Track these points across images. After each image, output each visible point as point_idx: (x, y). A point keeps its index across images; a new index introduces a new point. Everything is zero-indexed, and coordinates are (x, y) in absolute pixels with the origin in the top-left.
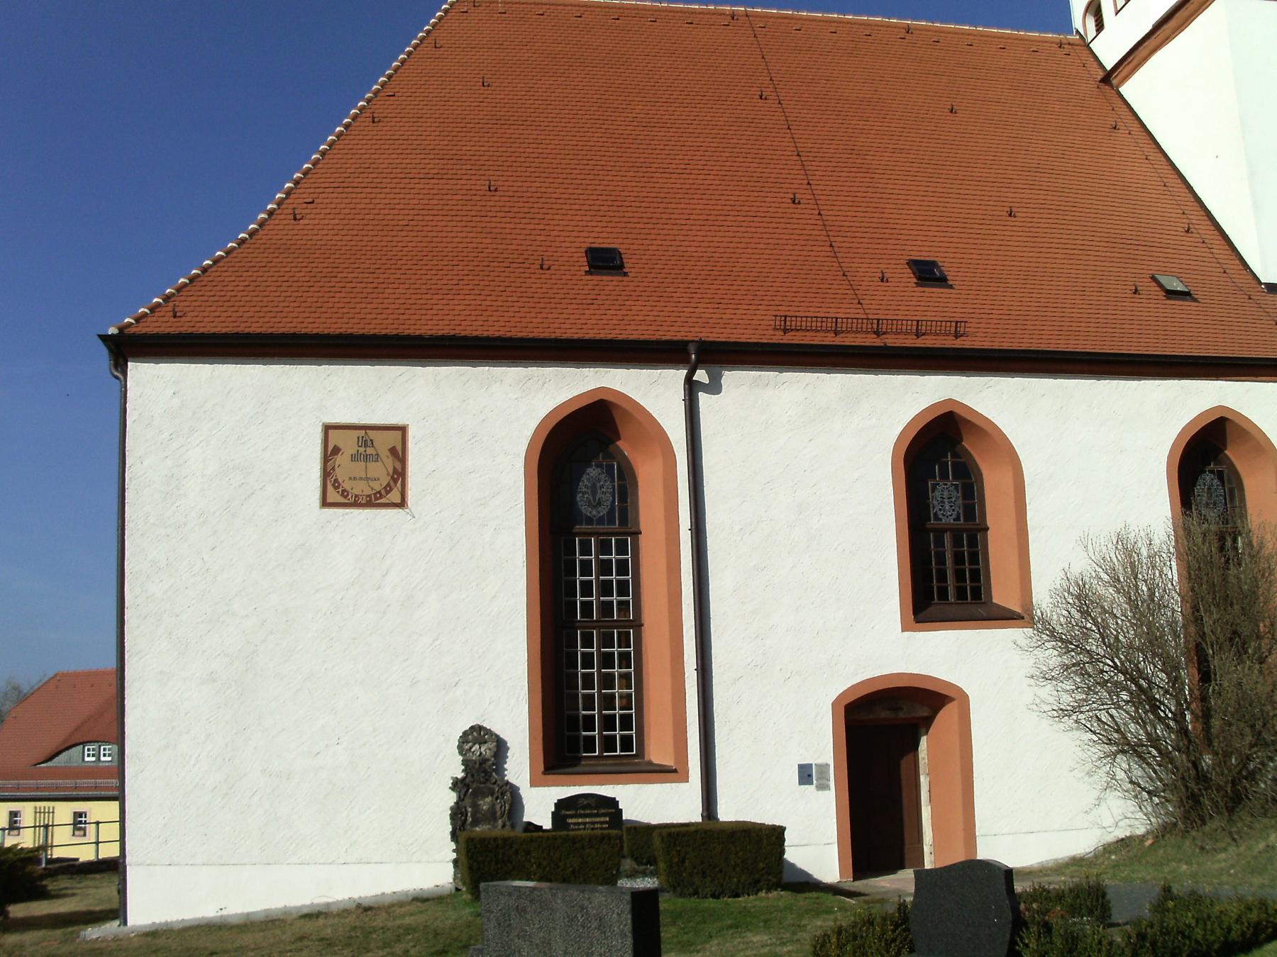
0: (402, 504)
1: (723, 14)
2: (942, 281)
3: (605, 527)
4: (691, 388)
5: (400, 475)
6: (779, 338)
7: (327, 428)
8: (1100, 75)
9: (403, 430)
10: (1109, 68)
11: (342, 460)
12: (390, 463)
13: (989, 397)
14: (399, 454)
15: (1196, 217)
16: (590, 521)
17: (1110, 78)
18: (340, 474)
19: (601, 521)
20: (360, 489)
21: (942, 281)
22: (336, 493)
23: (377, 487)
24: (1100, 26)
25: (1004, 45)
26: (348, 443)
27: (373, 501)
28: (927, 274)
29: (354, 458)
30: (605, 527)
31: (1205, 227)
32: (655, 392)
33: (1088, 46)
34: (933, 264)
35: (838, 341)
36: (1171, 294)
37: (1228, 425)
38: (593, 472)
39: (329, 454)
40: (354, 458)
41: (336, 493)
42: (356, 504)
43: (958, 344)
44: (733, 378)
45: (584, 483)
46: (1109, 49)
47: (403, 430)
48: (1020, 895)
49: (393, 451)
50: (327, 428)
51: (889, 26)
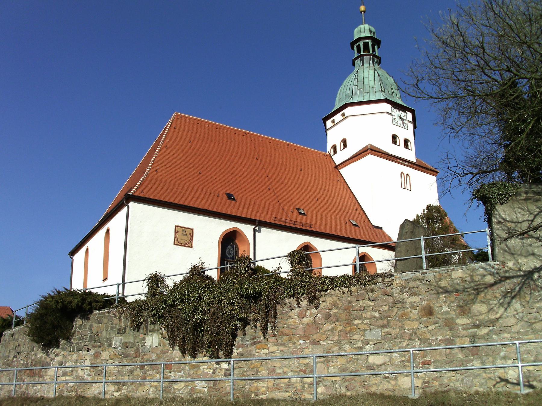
0: (191, 247)
1: (242, 132)
2: (234, 199)
3: (232, 260)
4: (255, 230)
5: (191, 240)
6: (274, 222)
7: (176, 226)
8: (334, 166)
9: (193, 229)
10: (337, 164)
11: (178, 234)
12: (189, 237)
13: (318, 243)
14: (191, 236)
15: (358, 207)
16: (228, 258)
17: (337, 167)
18: (178, 238)
19: (231, 258)
20: (183, 242)
21: (234, 199)
22: (177, 242)
23: (187, 242)
24: (335, 152)
25: (312, 153)
26: (180, 230)
27: (185, 245)
28: (230, 197)
29: (182, 234)
30: (232, 260)
31: (359, 209)
32: (247, 230)
33: (331, 157)
34: (232, 195)
35: (286, 224)
36: (354, 225)
37: (238, 238)
38: (229, 247)
39: (176, 233)
40: (182, 234)
41: (177, 242)
42: (181, 245)
43: (311, 229)
44: (263, 229)
45: (228, 249)
46: (338, 159)
47: (193, 229)
48: (72, 320)
49: (190, 234)
50: (176, 226)
51: (283, 143)
